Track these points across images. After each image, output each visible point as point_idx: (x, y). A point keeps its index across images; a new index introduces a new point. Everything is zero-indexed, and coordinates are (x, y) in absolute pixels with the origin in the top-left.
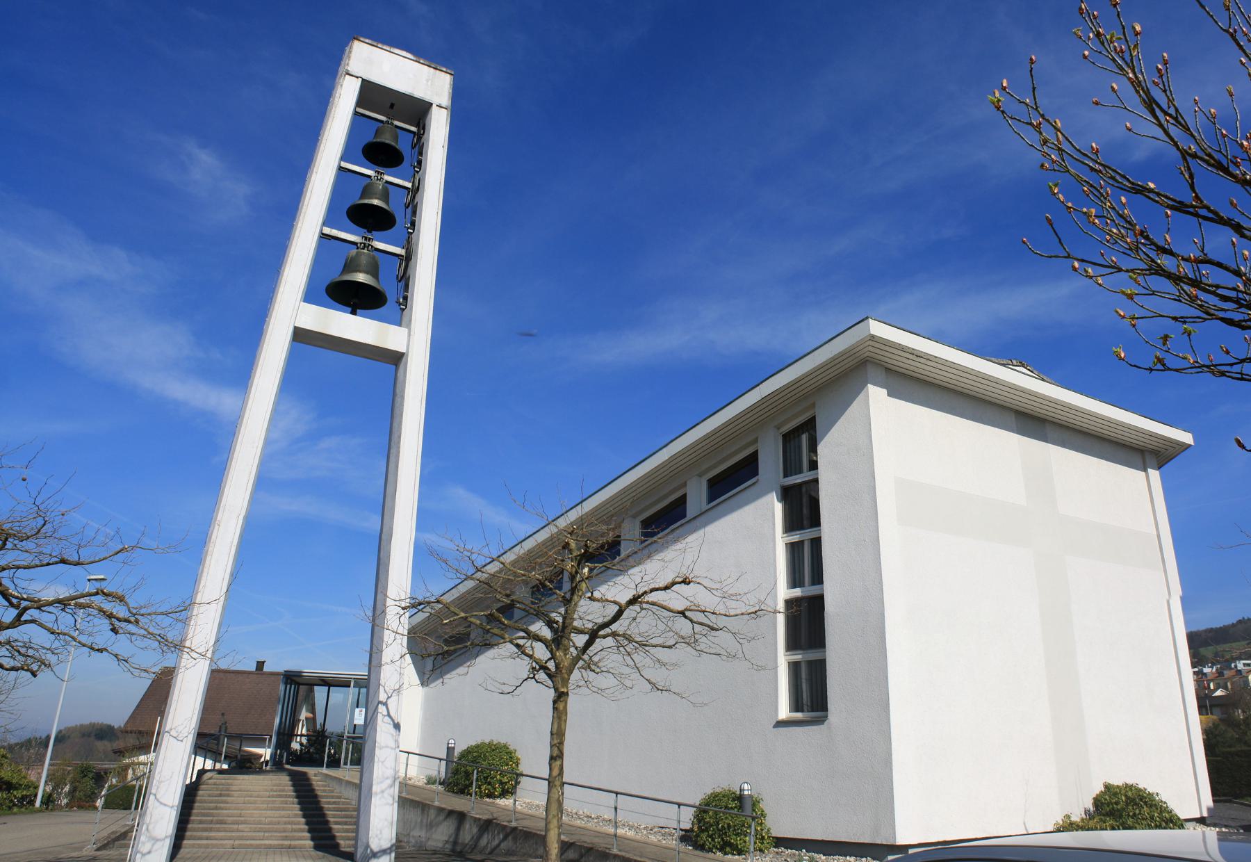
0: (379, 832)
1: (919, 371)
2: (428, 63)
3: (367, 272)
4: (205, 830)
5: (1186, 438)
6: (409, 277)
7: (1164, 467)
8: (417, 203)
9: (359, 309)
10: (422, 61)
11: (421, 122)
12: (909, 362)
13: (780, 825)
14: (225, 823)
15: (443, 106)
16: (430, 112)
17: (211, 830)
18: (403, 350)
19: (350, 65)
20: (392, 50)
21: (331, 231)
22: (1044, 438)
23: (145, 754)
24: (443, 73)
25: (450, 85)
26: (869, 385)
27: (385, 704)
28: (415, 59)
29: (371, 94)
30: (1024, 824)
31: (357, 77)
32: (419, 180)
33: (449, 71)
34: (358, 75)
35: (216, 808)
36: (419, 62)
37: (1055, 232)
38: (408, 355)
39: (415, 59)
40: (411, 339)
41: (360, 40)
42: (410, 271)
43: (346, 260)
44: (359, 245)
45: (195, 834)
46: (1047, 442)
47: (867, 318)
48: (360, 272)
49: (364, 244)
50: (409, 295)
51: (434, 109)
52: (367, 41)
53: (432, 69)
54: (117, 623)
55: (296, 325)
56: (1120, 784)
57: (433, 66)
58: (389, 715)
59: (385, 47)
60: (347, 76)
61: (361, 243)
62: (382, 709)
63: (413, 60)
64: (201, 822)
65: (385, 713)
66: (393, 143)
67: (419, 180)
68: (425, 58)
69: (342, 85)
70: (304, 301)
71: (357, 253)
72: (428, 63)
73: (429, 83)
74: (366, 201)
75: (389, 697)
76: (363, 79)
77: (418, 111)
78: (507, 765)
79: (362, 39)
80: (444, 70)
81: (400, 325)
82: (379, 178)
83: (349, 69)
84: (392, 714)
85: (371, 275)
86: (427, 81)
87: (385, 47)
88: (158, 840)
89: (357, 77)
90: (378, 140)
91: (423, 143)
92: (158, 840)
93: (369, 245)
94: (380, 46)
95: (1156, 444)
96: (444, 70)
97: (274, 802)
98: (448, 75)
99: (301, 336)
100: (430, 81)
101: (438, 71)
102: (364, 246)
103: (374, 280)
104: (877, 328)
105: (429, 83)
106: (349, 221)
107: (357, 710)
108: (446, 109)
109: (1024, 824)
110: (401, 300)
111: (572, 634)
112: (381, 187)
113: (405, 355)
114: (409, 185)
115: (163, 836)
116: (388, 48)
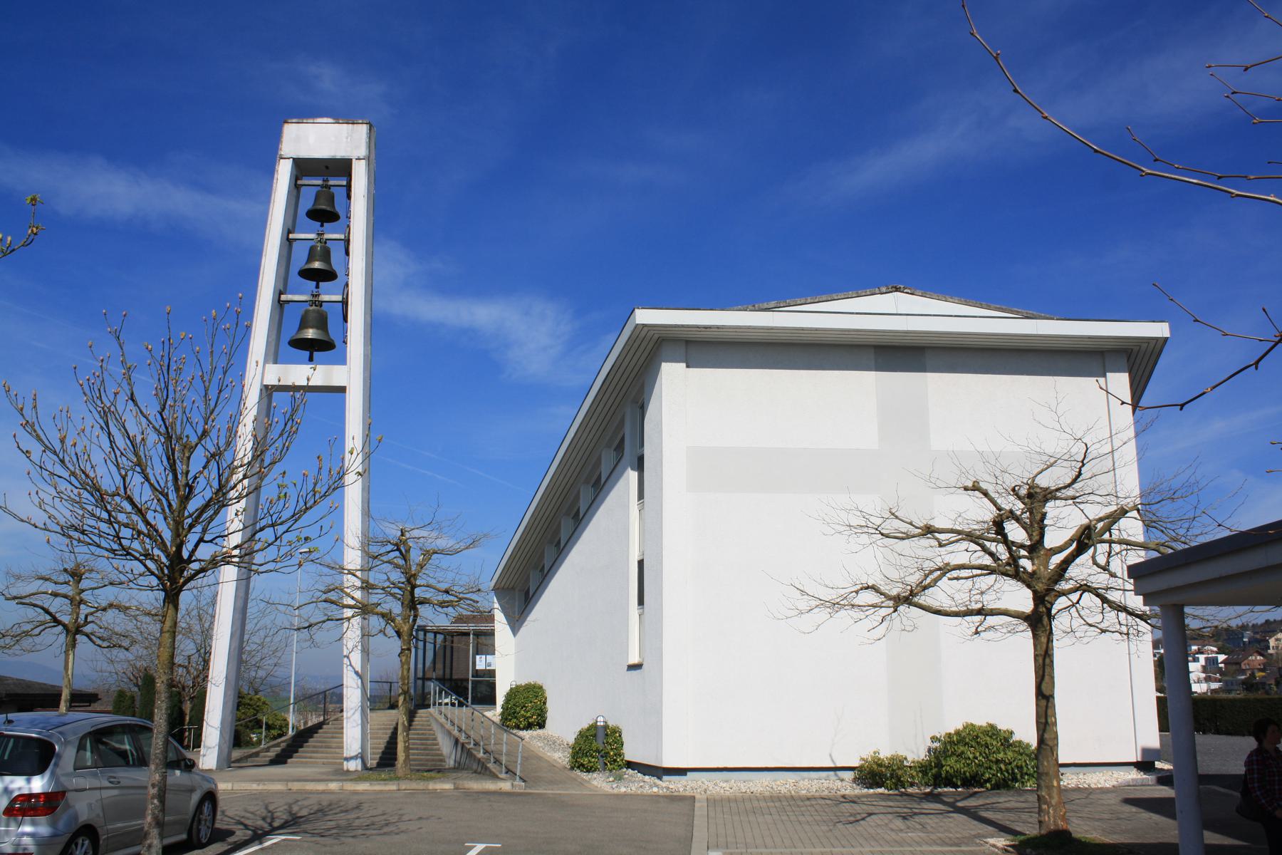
1: (724, 337)
4: (313, 752)
5: (1159, 330)
7: (1159, 362)
10: (341, 122)
12: (702, 333)
13: (630, 753)
14: (331, 748)
15: (362, 157)
17: (317, 752)
22: (923, 369)
24: (361, 125)
26: (664, 365)
27: (348, 657)
29: (303, 167)
30: (830, 755)
34: (288, 156)
35: (333, 737)
41: (288, 123)
45: (304, 754)
46: (925, 371)
47: (634, 310)
51: (355, 163)
52: (294, 121)
54: (1070, 492)
55: (265, 383)
56: (984, 724)
58: (351, 665)
59: (309, 121)
62: (346, 660)
64: (314, 747)
65: (348, 664)
69: (277, 171)
73: (349, 140)
75: (350, 653)
76: (294, 159)
77: (342, 167)
78: (531, 702)
83: (282, 153)
84: (353, 664)
87: (309, 121)
88: (210, 748)
89: (289, 158)
92: (210, 748)
94: (305, 121)
95: (1122, 344)
96: (360, 121)
97: (377, 733)
99: (269, 391)
100: (349, 138)
101: (355, 125)
103: (320, 332)
104: (645, 316)
105: (349, 140)
107: (478, 657)
109: (830, 755)
111: (418, 606)
114: (342, 237)
115: (214, 745)
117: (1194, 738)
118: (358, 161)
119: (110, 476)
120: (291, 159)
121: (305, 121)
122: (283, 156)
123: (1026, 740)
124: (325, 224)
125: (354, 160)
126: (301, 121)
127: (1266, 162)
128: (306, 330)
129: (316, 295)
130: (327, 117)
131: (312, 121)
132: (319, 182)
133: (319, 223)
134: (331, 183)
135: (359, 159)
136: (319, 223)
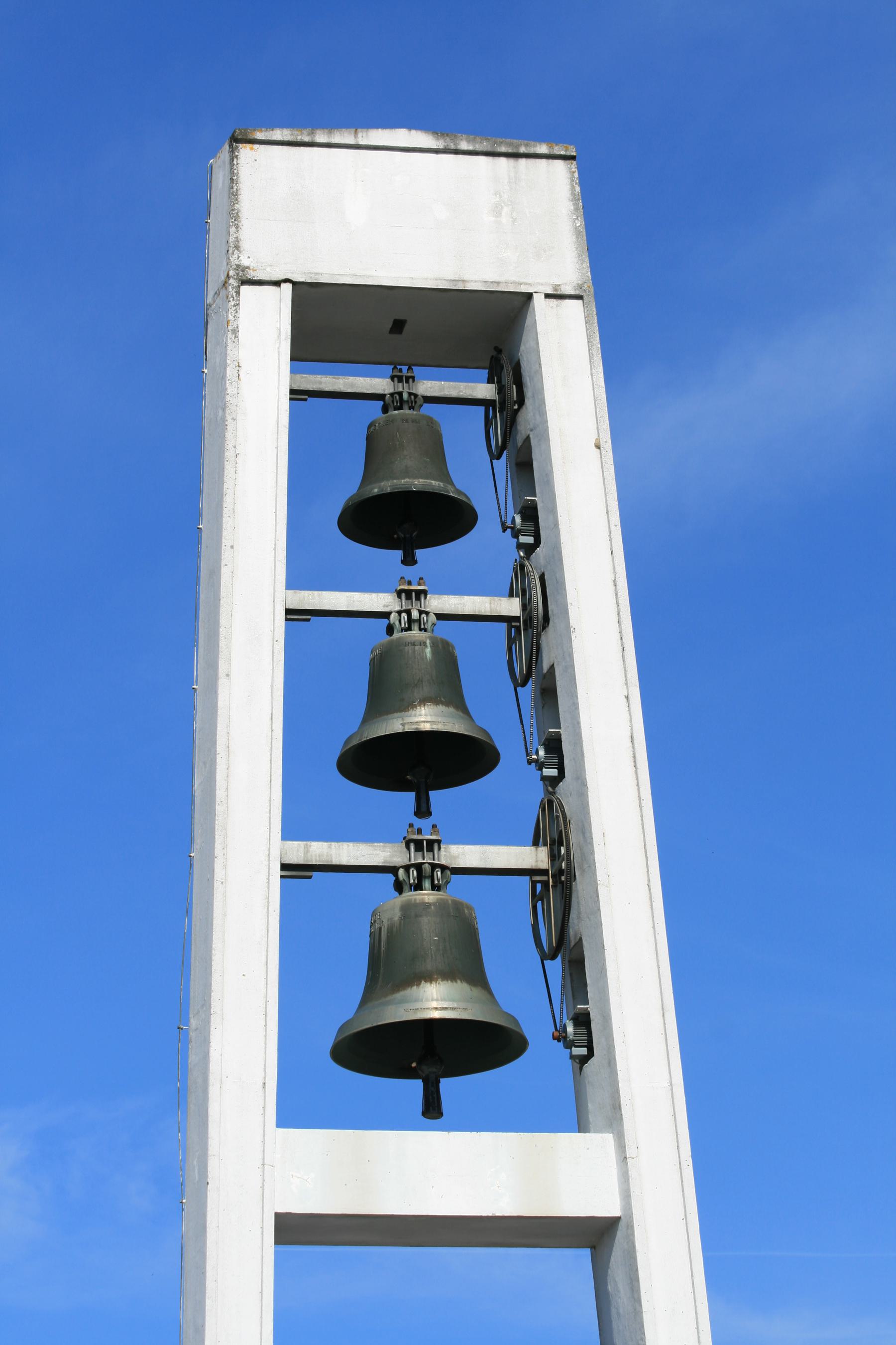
0: (227, 460)
2: (484, 146)
3: (434, 700)
6: (580, 942)
8: (552, 667)
9: (417, 549)
10: (464, 146)
11: (504, 357)
15: (568, 290)
16: (528, 322)
18: (615, 1212)
19: (244, 245)
20: (362, 141)
21: (307, 851)
23: (576, 1012)
24: (544, 162)
25: (574, 199)
28: (439, 144)
31: (277, 283)
32: (542, 578)
33: (559, 150)
36: (457, 152)
37: (693, 1287)
38: (630, 1227)
39: (439, 144)
40: (632, 1172)
42: (578, 925)
43: (375, 937)
44: (401, 872)
48: (429, 977)
49: (419, 867)
50: (592, 1008)
52: (278, 134)
53: (503, 160)
57: (503, 149)
59: (337, 138)
60: (245, 289)
61: (407, 868)
63: (437, 151)
66: (435, 485)
67: (542, 578)
68: (473, 132)
69: (235, 332)
70: (283, 1121)
71: (407, 909)
72: (484, 146)
73: (504, 219)
74: (396, 725)
76: (294, 284)
79: (259, 136)
80: (543, 149)
81: (582, 1126)
82: (415, 614)
83: (245, 262)
85: (447, 704)
86: (497, 211)
87: (337, 138)
89: (277, 283)
90: (387, 486)
91: (528, 439)
93: (434, 866)
94: (321, 138)
96: (543, 149)
98: (559, 164)
100: (506, 210)
101: (523, 162)
102: (420, 877)
105: (504, 219)
106: (341, 776)
108: (579, 297)
110: (570, 1029)
112: (428, 651)
113: (622, 1225)
116: (346, 137)
117: (521, 446)
118: (553, 302)
119: (263, 1050)
120: (287, 288)
121: (321, 138)
122: (252, 275)
123: (487, 372)
124: (420, 553)
125: (539, 301)
126: (306, 139)
127: (279, 641)
128: (413, 991)
129: (431, 843)
130: (411, 125)
131: (350, 140)
132: (381, 384)
133: (398, 554)
134: (427, 386)
135: (555, 296)
136: (398, 554)
